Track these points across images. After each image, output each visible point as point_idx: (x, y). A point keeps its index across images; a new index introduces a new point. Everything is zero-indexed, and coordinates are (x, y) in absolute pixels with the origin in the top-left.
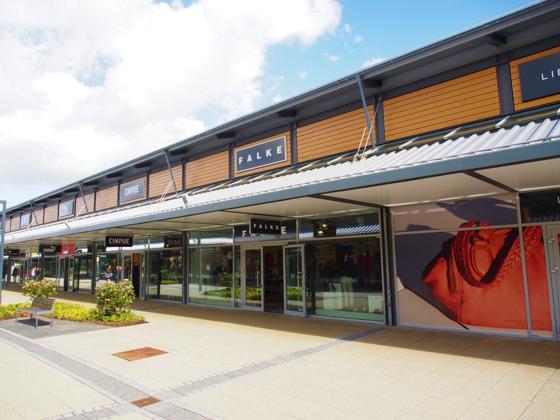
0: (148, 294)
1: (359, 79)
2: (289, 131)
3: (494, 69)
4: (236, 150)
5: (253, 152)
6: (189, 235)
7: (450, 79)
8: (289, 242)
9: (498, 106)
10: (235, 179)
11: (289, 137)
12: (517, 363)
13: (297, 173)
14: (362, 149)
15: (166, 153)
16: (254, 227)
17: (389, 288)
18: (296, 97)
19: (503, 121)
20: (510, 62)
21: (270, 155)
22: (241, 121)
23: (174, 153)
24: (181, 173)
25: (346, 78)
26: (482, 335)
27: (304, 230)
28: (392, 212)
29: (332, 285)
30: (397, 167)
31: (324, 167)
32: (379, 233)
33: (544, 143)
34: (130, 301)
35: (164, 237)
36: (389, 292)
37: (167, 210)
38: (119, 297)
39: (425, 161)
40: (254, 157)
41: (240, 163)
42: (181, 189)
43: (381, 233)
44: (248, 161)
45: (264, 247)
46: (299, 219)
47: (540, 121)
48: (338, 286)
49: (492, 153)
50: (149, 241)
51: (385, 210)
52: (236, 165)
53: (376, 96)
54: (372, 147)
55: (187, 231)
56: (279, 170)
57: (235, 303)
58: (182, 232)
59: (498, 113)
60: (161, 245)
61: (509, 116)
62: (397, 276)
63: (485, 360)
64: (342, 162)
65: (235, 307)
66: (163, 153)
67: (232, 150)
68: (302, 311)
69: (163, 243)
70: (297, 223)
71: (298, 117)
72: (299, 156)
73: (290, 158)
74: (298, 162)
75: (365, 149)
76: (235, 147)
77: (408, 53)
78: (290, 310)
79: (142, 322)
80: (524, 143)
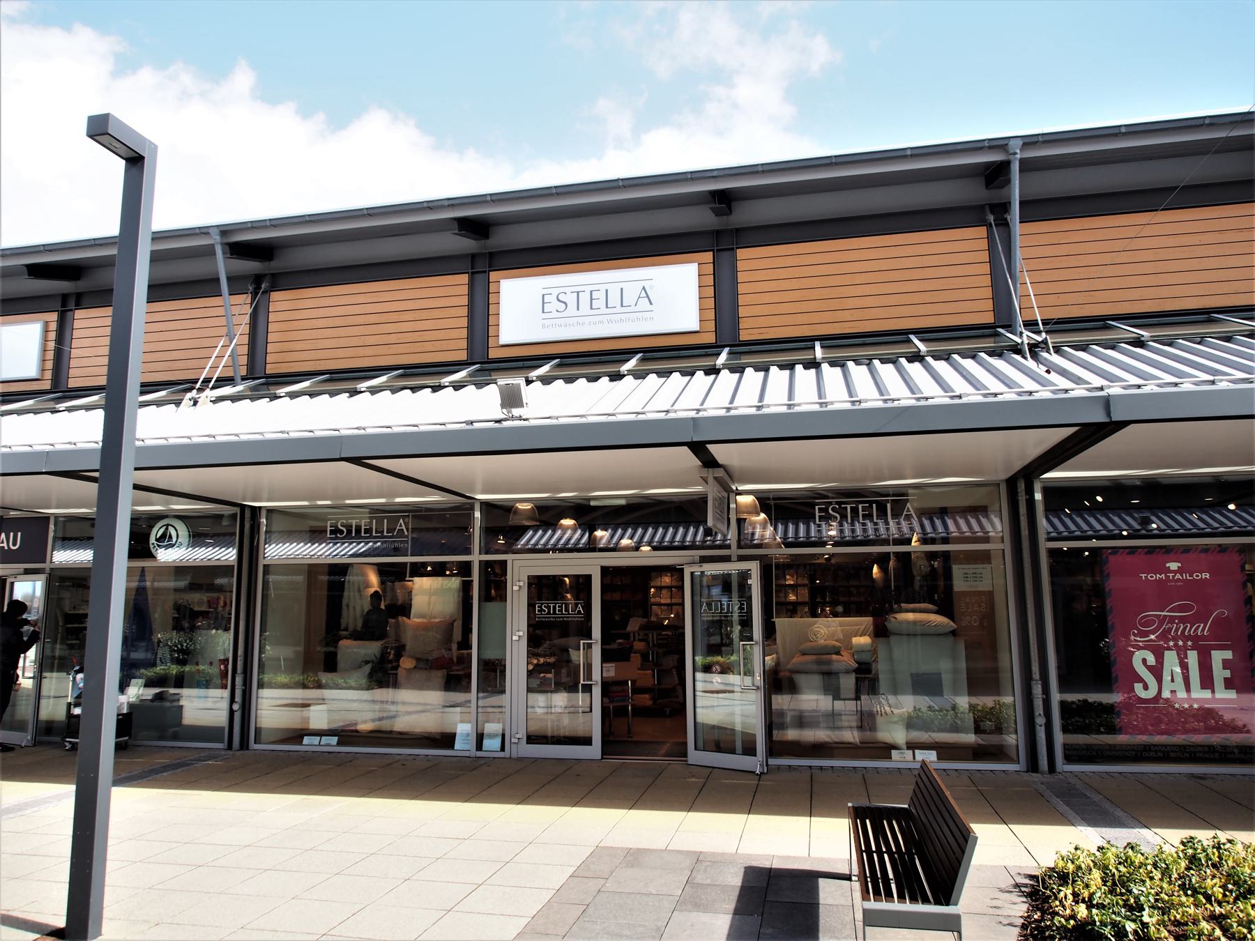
1: (218, 238)
3: (464, 278)
8: (25, 569)
9: (464, 344)
12: (685, 811)
14: (207, 381)
19: (631, 364)
20: (490, 273)
22: (365, 215)
23: (239, 250)
26: (298, 753)
36: (239, 680)
45: (605, 570)
46: (57, 517)
53: (258, 279)
54: (233, 380)
55: (260, 508)
59: (463, 356)
63: (519, 806)
71: (276, 265)
72: (72, 372)
75: (211, 386)
80: (638, 413)
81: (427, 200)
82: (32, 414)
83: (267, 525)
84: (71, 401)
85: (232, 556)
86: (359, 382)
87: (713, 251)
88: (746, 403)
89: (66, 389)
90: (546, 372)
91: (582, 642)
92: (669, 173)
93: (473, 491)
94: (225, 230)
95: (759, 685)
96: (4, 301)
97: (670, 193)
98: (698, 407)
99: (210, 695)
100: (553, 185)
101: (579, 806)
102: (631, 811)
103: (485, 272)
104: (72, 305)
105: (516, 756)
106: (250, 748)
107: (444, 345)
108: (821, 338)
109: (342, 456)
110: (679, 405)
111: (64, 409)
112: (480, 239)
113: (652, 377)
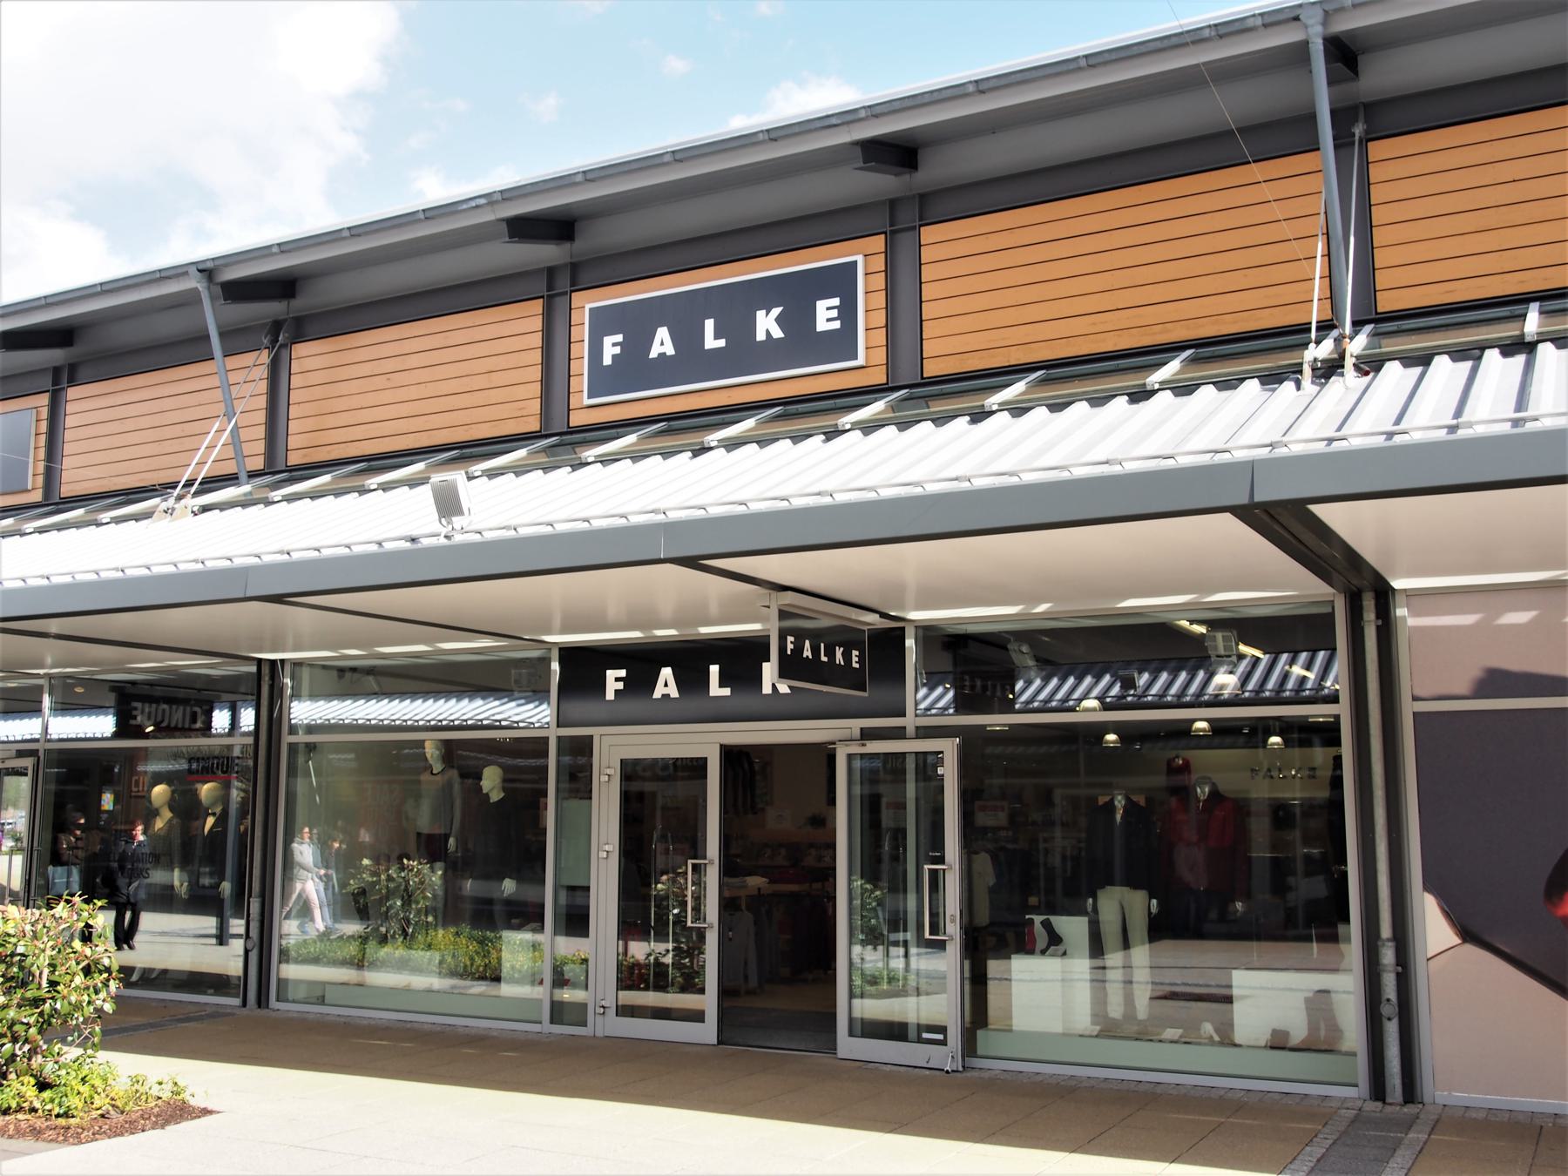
2: (541, 300)
3: (537, 306)
4: (586, 304)
5: (636, 323)
6: (292, 679)
7: (633, 277)
10: (571, 433)
11: (879, 263)
12: (1167, 1162)
13: (828, 439)
14: (189, 484)
15: (209, 288)
16: (789, 652)
17: (1388, 940)
18: (505, 190)
19: (1171, 369)
21: (777, 333)
23: (239, 291)
25: (1254, 16)
26: (451, 1027)
28: (1401, 612)
29: (1047, 925)
30: (1011, 474)
32: (1333, 699)
33: (1272, 455)
34: (99, 1003)
37: (348, 547)
38: (58, 983)
39: (827, 492)
40: (687, 338)
41: (607, 361)
43: (1345, 698)
44: (653, 354)
48: (1073, 927)
49: (627, 527)
50: (47, 701)
51: (1372, 603)
52: (582, 367)
55: (282, 661)
56: (315, 471)
57: (553, 1003)
60: (101, 726)
61: (1043, 372)
62: (1428, 887)
64: (637, 456)
65: (552, 1022)
66: (194, 283)
68: (943, 1043)
69: (106, 714)
70: (910, 643)
71: (301, 304)
72: (293, 442)
73: (880, 356)
75: (1313, 335)
76: (576, 286)
77: (1029, 66)
79: (177, 1111)
80: (1216, 452)
81: (160, 268)
82: (240, 508)
83: (292, 688)
84: (291, 485)
85: (546, 716)
86: (472, 463)
87: (885, 233)
88: (1365, 431)
92: (88, 284)
93: (902, 607)
94: (207, 271)
95: (953, 933)
96: (5, 378)
97: (477, 222)
98: (1331, 433)
100: (42, 295)
101: (1179, 1162)
102: (1173, 1165)
103: (914, 228)
104: (563, 282)
105: (602, 1035)
106: (270, 1006)
108: (1542, 297)
109: (248, 595)
110: (1412, 420)
111: (280, 498)
113: (1208, 391)
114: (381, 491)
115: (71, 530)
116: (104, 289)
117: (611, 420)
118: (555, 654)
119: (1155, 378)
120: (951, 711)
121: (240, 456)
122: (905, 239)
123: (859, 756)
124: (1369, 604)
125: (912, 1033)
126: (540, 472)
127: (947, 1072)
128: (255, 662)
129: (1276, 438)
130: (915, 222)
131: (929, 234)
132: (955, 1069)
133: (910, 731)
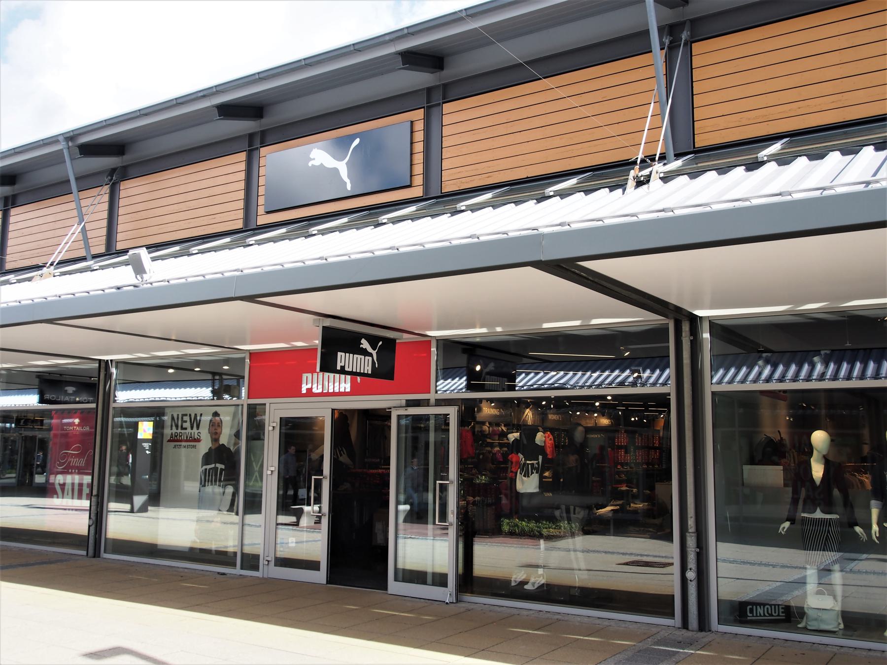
0: (243, 554)
2: (245, 152)
8: (407, 401)
20: (693, 44)
23: (90, 150)
24: (106, 206)
27: (448, 372)
31: (373, 227)
35: (38, 377)
36: (691, 542)
42: (102, 249)
47: (851, 150)
58: (97, 365)
64: (413, 218)
67: (256, 153)
70: (434, 350)
72: (8, 258)
74: (258, 224)
78: (281, 566)
89: (255, 227)
90: (779, 151)
91: (313, 477)
98: (869, 178)
99: (160, 517)
107: (194, 223)
112: (256, 120)
114: (469, 212)
115: (87, 272)
116: (16, 151)
117: (223, 231)
118: (247, 356)
119: (764, 154)
120: (464, 390)
121: (87, 247)
122: (435, 111)
123: (404, 416)
124: (686, 327)
125: (429, 579)
126: (491, 208)
127: (447, 603)
128: (98, 362)
129: (826, 184)
130: (440, 100)
131: (447, 107)
132: (452, 601)
133: (432, 401)
